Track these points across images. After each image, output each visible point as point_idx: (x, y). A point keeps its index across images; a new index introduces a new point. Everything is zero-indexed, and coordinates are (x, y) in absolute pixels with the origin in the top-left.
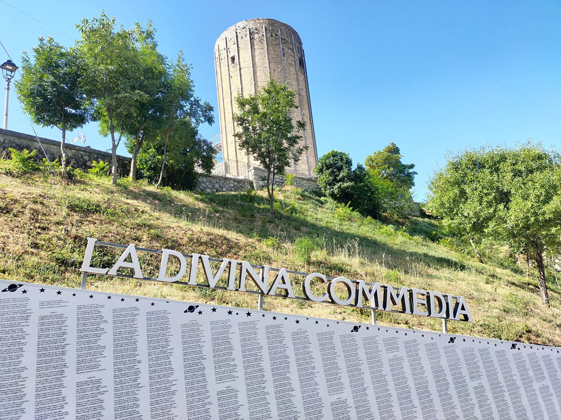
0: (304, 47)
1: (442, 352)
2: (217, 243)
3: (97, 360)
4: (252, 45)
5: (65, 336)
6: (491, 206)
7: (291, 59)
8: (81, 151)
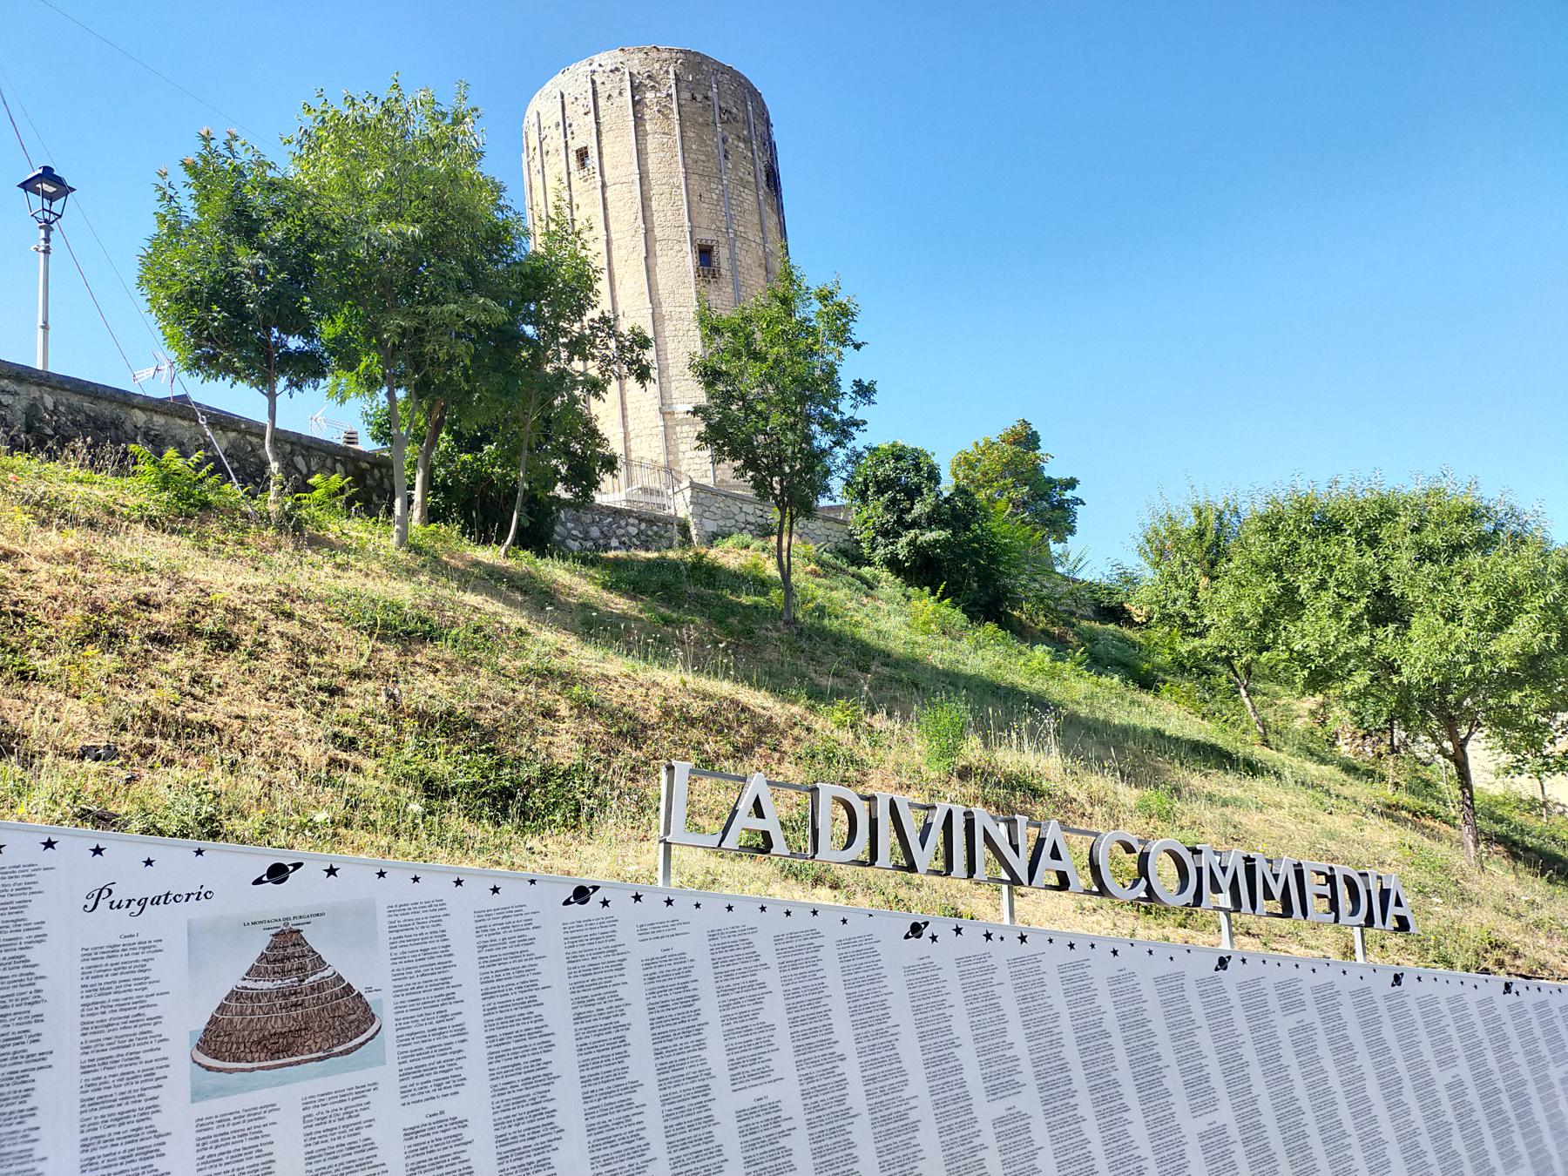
0: (775, 138)
1: (1382, 1006)
2: (727, 719)
3: (766, 1057)
4: (639, 120)
5: (697, 1005)
6: (1360, 629)
7: (745, 169)
8: (252, 434)
